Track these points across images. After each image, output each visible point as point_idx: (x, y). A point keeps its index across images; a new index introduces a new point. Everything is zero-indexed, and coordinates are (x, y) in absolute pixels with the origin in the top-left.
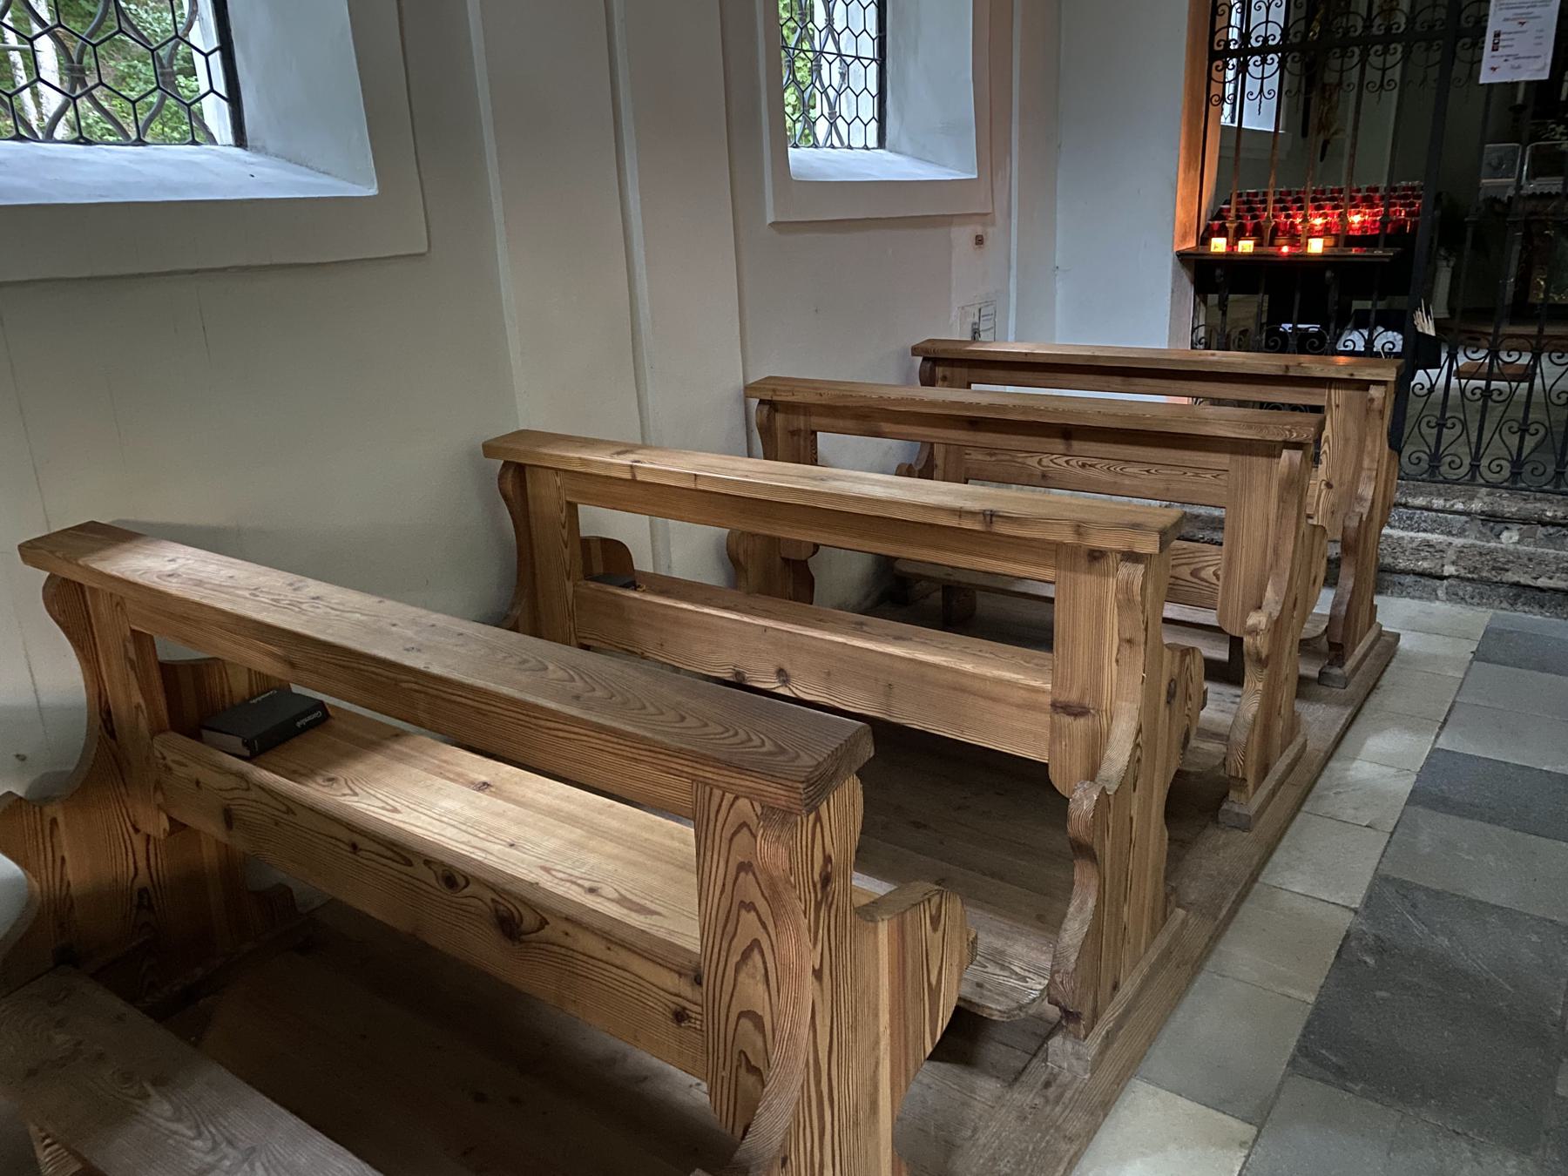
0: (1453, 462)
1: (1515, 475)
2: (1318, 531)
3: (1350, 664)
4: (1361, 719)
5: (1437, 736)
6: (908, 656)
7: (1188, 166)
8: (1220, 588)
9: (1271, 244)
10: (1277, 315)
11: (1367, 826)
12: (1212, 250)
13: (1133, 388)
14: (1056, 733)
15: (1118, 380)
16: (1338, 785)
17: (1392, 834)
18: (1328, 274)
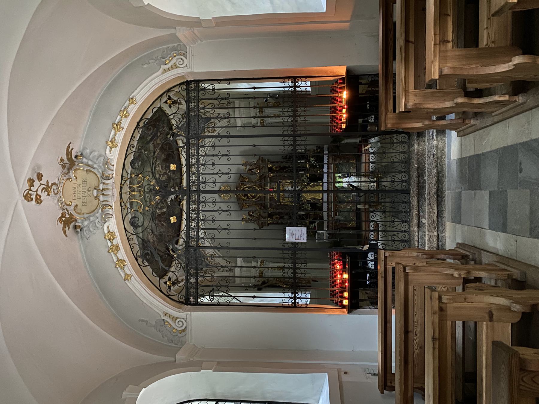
0: (404, 237)
1: (406, 222)
2: (427, 263)
3: (468, 253)
4: (485, 248)
5: (485, 229)
6: (485, 369)
7: (324, 312)
8: (449, 286)
9: (345, 288)
10: (365, 286)
11: (517, 242)
12: (347, 304)
13: (390, 321)
14: (499, 321)
15: (388, 325)
16: (506, 251)
17: (517, 235)
18: (353, 272)
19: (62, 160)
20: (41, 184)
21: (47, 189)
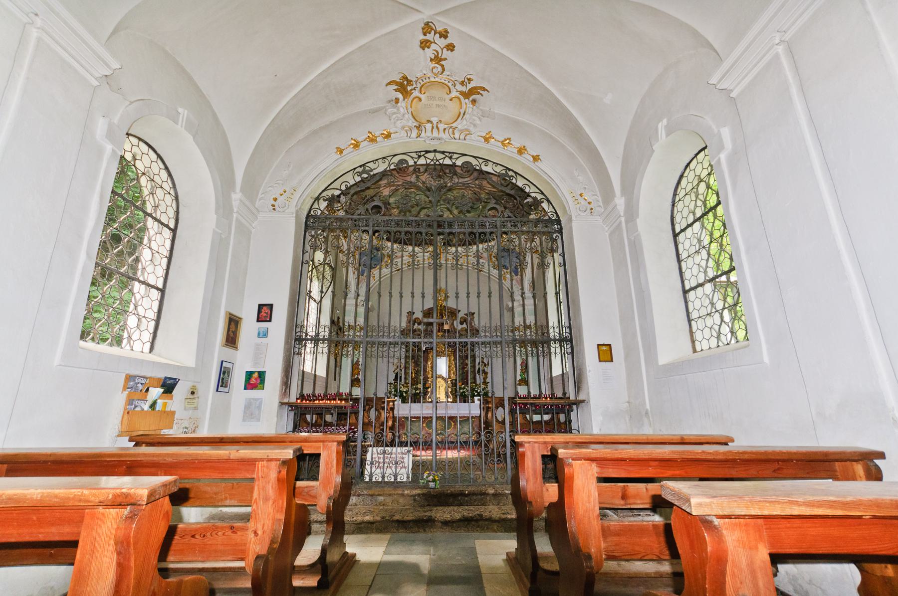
19: (470, 80)
20: (442, 50)
21: (437, 59)
